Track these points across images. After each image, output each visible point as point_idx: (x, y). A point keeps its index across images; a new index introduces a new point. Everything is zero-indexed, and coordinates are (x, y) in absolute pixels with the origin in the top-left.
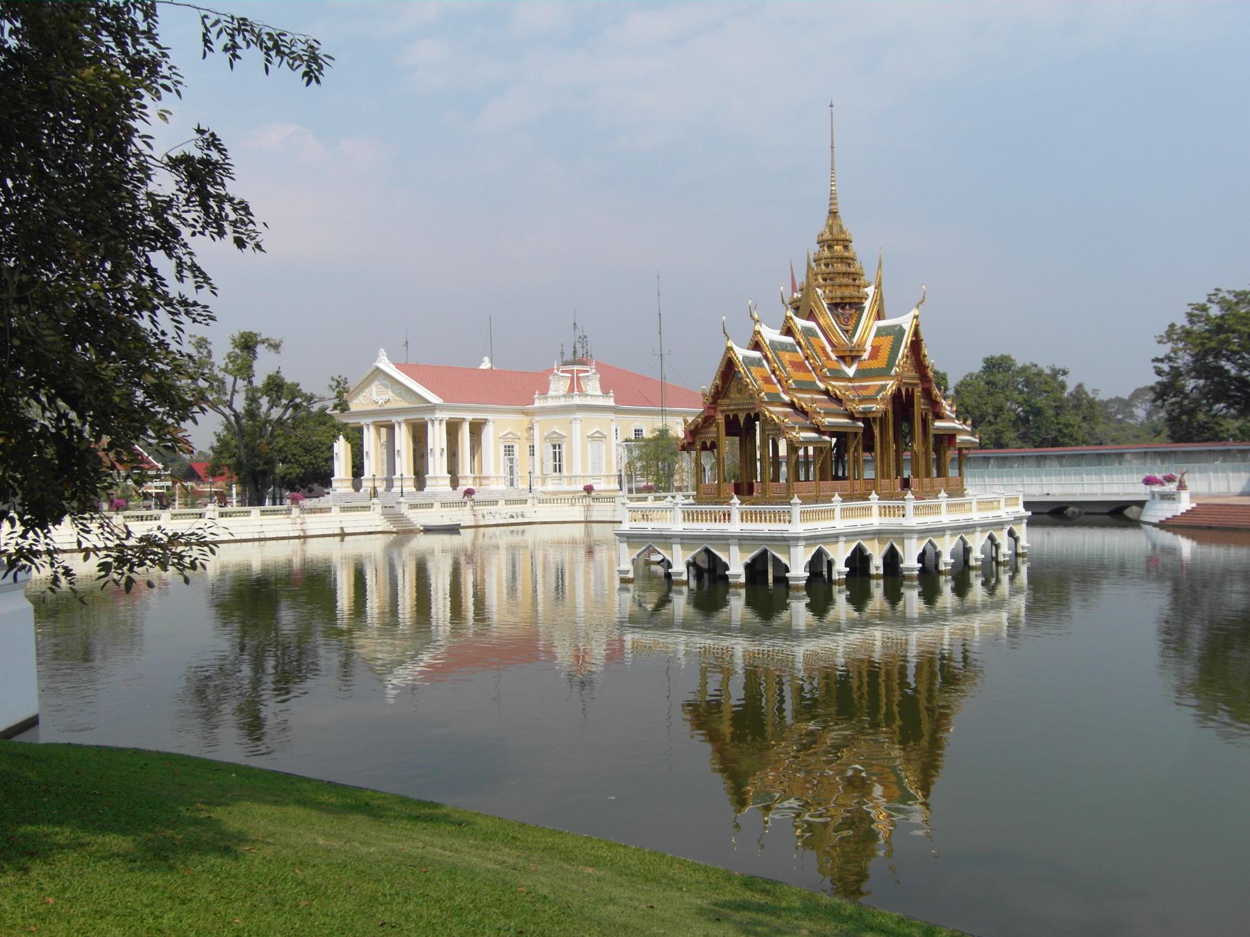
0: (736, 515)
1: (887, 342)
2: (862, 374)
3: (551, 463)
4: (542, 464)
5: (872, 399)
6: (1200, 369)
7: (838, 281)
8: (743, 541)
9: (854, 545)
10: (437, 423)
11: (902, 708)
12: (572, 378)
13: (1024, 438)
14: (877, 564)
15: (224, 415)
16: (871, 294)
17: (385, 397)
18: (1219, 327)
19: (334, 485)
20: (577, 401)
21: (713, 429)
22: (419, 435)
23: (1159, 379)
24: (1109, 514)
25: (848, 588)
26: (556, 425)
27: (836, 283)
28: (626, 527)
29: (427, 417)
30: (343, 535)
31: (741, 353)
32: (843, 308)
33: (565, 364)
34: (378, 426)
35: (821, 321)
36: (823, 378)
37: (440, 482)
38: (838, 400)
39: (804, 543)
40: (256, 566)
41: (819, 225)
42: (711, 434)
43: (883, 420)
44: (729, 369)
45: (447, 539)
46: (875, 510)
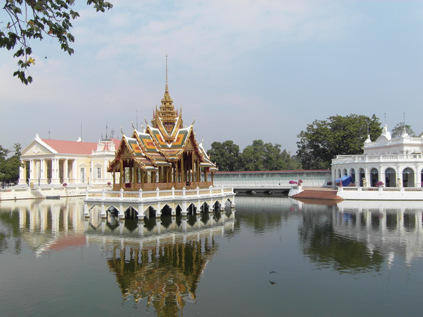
0: (122, 195)
1: (182, 136)
2: (174, 147)
3: (97, 175)
4: (94, 175)
5: (174, 155)
6: (312, 145)
7: (166, 115)
8: (124, 203)
9: (216, 201)
10: (55, 160)
11: (186, 260)
12: (105, 145)
13: (266, 167)
14: (174, 211)
16: (178, 120)
17: (38, 151)
18: (317, 132)
19: (365, 152)
20: (106, 153)
21: (119, 165)
22: (49, 164)
23: (299, 149)
25: (161, 220)
26: (99, 161)
27: (167, 115)
28: (87, 198)
29: (52, 158)
30: (15, 200)
31: (127, 139)
32: (168, 124)
33: (103, 140)
34: (36, 161)
35: (160, 129)
36: (158, 148)
37: (56, 181)
38: (163, 155)
39: (143, 204)
41: (162, 96)
42: (118, 166)
43: (179, 162)
44: (123, 145)
45: (56, 201)
46: (173, 193)
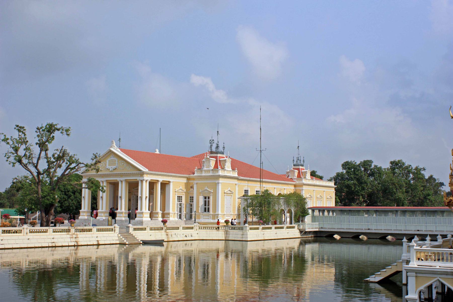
10: (144, 182)
15: (31, 172)
24: (352, 238)
29: (138, 178)
40: (49, 262)
45: (158, 249)
